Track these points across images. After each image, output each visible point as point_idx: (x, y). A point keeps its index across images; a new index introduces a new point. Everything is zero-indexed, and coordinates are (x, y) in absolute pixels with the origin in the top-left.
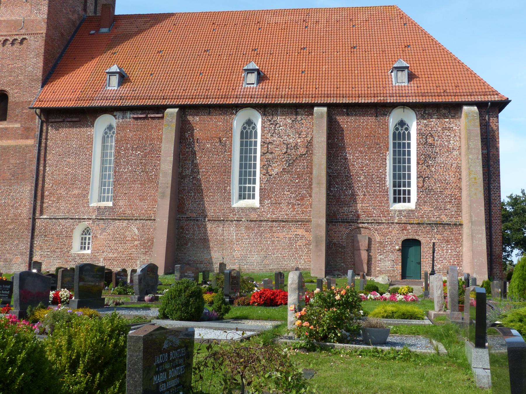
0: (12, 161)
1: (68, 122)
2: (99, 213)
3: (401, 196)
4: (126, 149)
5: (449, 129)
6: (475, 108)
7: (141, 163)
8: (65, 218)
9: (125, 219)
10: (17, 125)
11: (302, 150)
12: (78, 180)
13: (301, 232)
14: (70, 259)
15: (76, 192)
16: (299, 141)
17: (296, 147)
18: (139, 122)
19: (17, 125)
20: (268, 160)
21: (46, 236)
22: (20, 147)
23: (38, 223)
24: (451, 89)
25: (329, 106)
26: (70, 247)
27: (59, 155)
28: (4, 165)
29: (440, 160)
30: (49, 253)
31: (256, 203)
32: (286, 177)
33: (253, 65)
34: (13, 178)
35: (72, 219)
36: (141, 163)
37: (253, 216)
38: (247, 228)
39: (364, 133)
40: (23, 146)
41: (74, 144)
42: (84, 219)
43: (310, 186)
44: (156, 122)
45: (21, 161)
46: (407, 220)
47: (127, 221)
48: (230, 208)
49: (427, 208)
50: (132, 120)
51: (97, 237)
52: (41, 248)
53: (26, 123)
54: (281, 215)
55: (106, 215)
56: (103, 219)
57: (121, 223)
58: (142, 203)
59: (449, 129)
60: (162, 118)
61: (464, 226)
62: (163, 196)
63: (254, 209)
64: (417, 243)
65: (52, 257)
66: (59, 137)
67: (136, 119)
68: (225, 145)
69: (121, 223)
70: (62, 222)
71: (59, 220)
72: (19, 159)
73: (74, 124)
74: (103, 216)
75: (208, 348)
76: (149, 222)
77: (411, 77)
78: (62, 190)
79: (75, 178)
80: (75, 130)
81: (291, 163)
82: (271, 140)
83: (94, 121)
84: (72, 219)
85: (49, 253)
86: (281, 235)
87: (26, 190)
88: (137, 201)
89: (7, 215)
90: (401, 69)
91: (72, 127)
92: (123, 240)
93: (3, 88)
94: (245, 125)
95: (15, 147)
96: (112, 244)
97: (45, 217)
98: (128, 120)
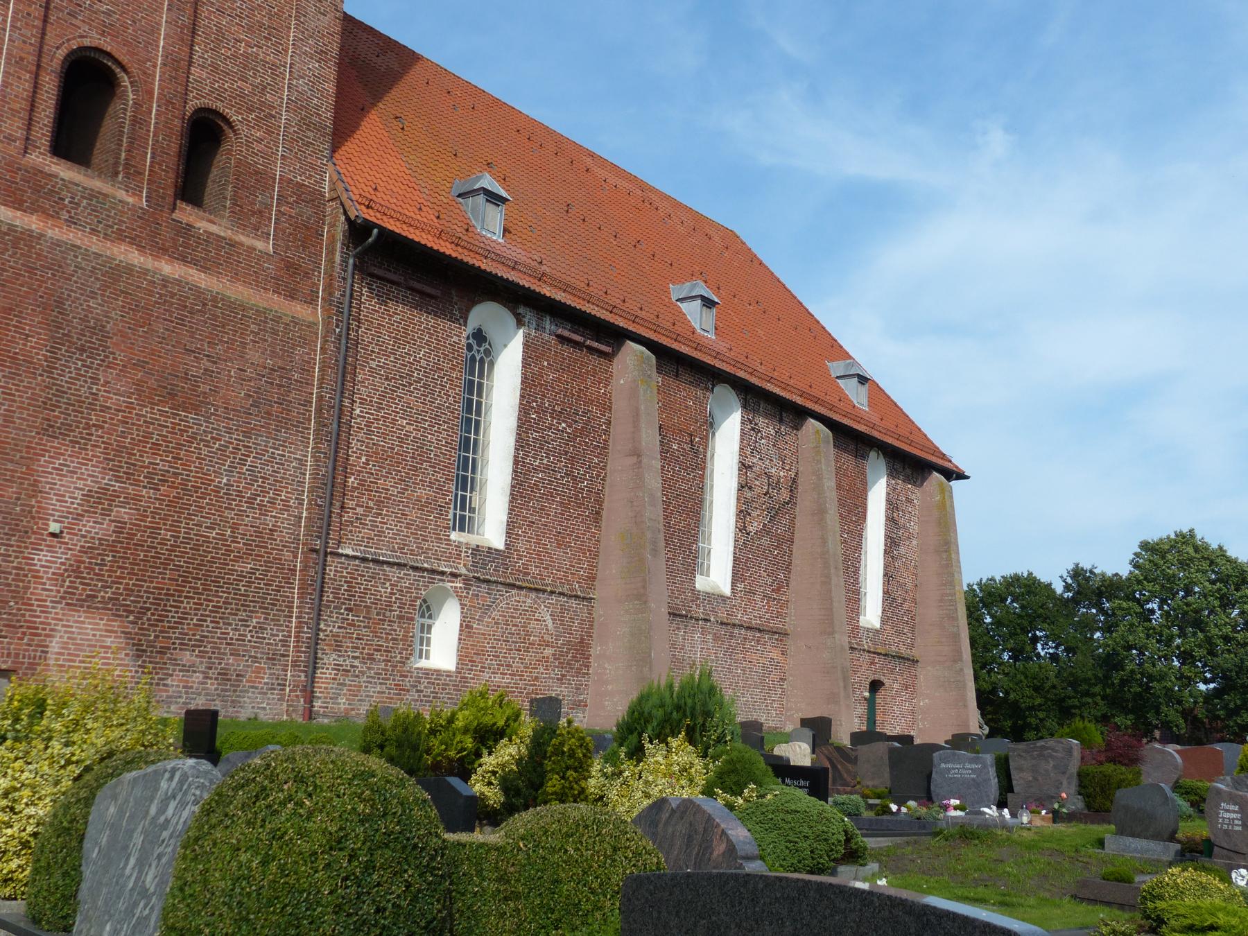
0: (254, 355)
1: (409, 288)
2: (475, 564)
7: (566, 453)
8: (399, 565)
9: (531, 589)
12: (428, 460)
14: (407, 683)
15: (423, 492)
16: (782, 474)
18: (567, 351)
21: (349, 610)
22: (277, 319)
27: (387, 379)
28: (230, 360)
30: (356, 663)
34: (254, 410)
35: (415, 569)
36: (566, 453)
38: (716, 637)
40: (287, 320)
42: (443, 573)
44: (594, 360)
45: (280, 363)
47: (533, 595)
48: (693, 590)
50: (553, 341)
51: (471, 627)
52: (338, 647)
53: (288, 248)
55: (490, 571)
56: (488, 581)
57: (522, 599)
58: (559, 553)
60: (609, 357)
61: (664, 610)
65: (363, 673)
66: (398, 331)
67: (562, 339)
68: (696, 453)
69: (522, 599)
71: (385, 567)
72: (274, 354)
73: (424, 301)
76: (573, 603)
78: (389, 483)
80: (425, 320)
83: (468, 310)
84: (415, 569)
85: (356, 663)
87: (300, 460)
89: (234, 527)
91: (418, 306)
93: (219, 104)
94: (471, 341)
97: (349, 552)
98: (547, 337)
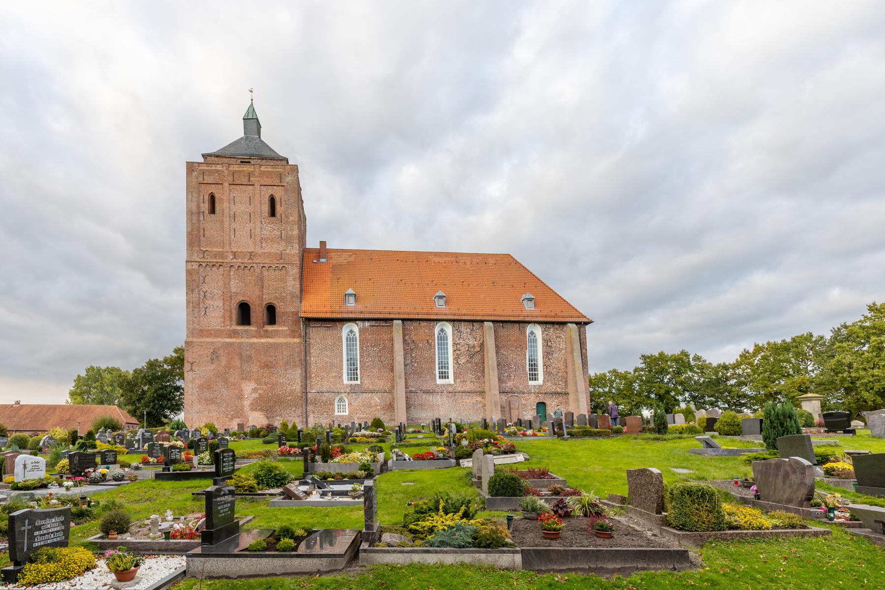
0: (285, 353)
3: (534, 377)
4: (367, 346)
5: (560, 337)
6: (491, 324)
10: (285, 328)
11: (477, 349)
13: (479, 399)
15: (334, 374)
17: (474, 347)
19: (285, 328)
20: (458, 355)
23: (309, 395)
24: (559, 314)
25: (403, 320)
26: (334, 411)
29: (555, 355)
31: (451, 380)
32: (469, 365)
33: (440, 293)
37: (450, 389)
39: (513, 339)
41: (329, 342)
43: (483, 371)
46: (539, 391)
49: (549, 384)
52: (313, 412)
54: (467, 389)
59: (560, 337)
62: (400, 377)
63: (451, 385)
64: (544, 404)
70: (327, 394)
74: (354, 391)
75: (848, 391)
77: (446, 303)
79: (332, 365)
80: (329, 332)
81: (472, 356)
82: (458, 342)
86: (468, 401)
88: (377, 381)
90: (441, 297)
92: (370, 406)
95: (286, 344)
96: (362, 408)
